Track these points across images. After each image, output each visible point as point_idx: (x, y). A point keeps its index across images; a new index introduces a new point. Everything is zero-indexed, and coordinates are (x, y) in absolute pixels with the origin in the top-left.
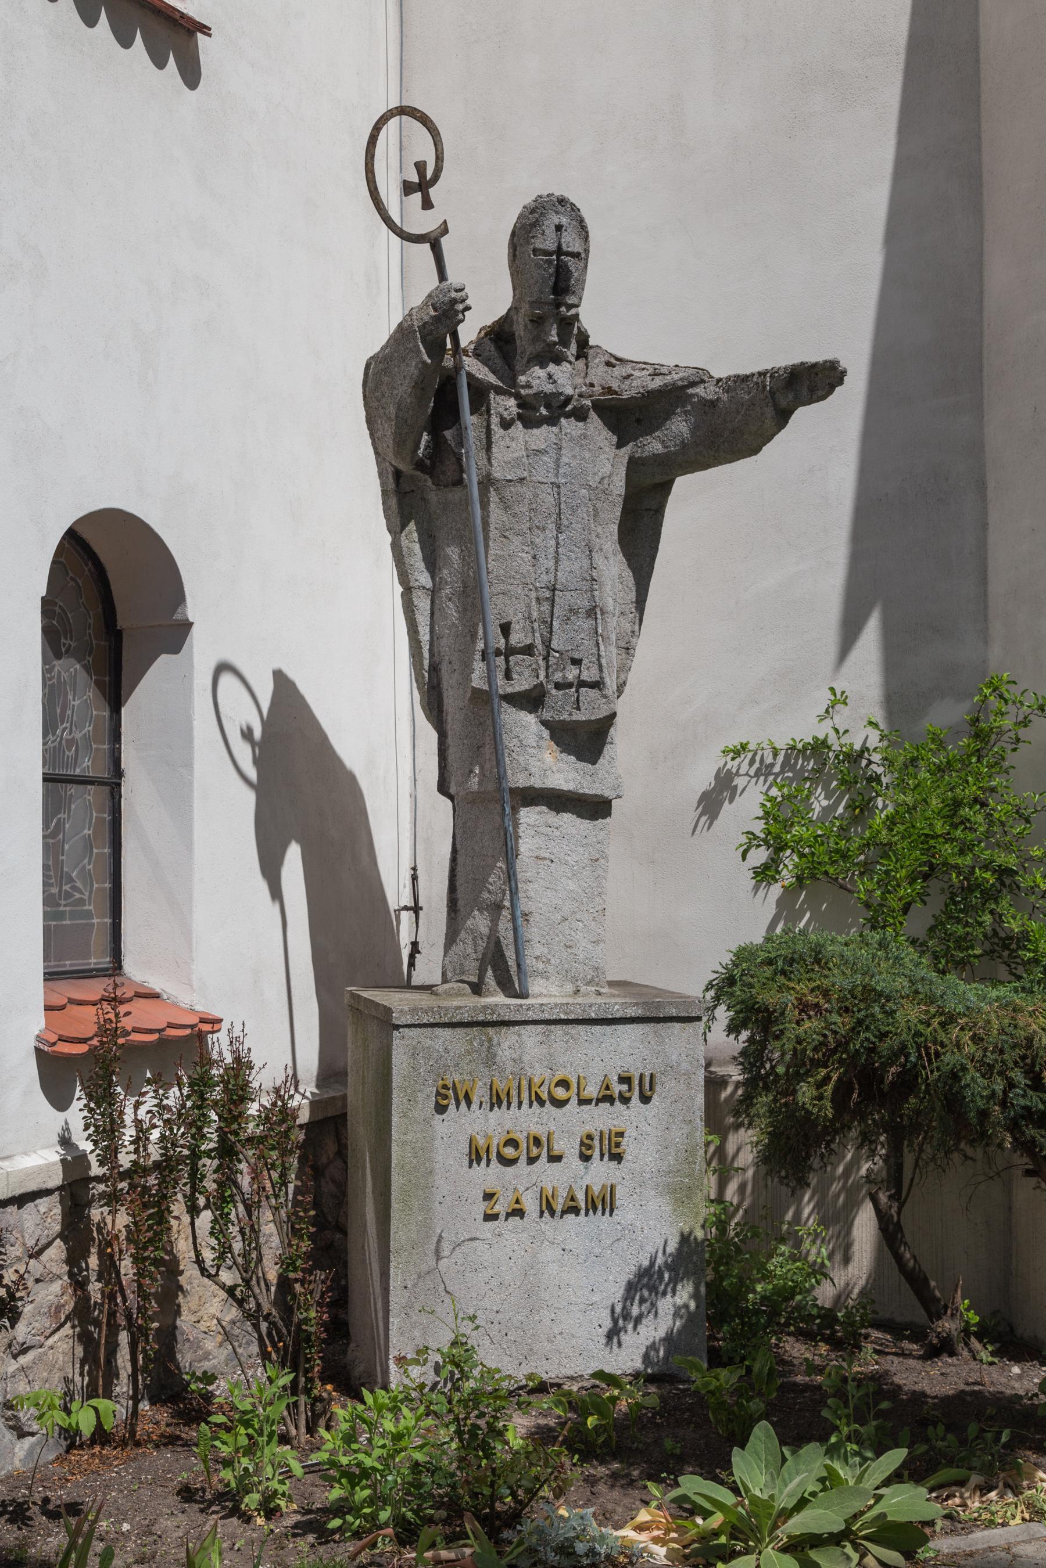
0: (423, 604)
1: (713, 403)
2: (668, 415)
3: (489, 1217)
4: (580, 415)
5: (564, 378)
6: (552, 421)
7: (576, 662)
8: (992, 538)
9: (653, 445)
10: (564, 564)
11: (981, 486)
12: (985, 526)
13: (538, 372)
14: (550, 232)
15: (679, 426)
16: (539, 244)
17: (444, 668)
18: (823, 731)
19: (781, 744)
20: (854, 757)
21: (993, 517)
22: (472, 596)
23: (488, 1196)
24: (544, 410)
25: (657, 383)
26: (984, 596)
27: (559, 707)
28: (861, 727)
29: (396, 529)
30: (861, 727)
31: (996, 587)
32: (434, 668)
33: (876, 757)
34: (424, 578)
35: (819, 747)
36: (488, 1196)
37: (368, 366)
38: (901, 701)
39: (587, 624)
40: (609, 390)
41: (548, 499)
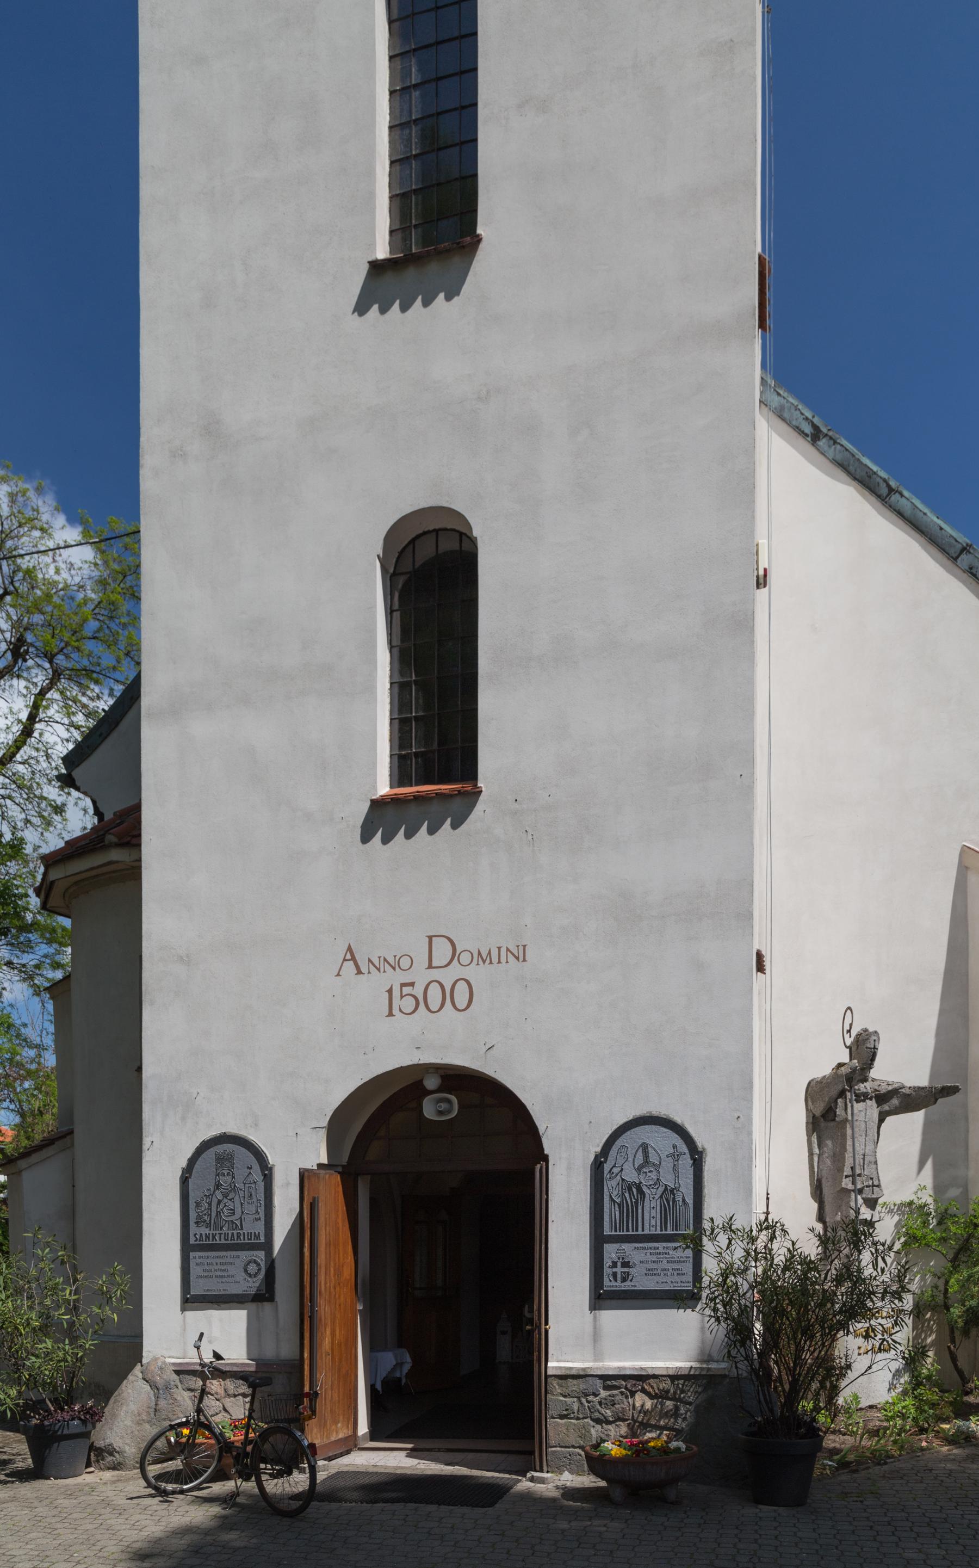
0: (816, 1159)
1: (909, 1095)
2: (892, 1098)
3: (859, 1354)
4: (871, 1099)
5: (862, 1087)
6: (864, 1101)
7: (872, 1179)
8: (971, 1135)
9: (886, 1107)
10: (868, 1148)
11: (967, 1119)
12: (968, 1131)
13: (862, 1085)
14: (872, 1042)
15: (895, 1102)
16: (868, 1045)
17: (824, 1181)
18: (913, 1197)
19: (898, 1202)
20: (922, 1207)
21: (971, 1128)
22: (838, 1158)
23: (859, 1348)
24: (862, 1097)
25: (890, 1088)
26: (967, 1154)
27: (867, 1193)
28: (927, 1198)
29: (809, 1136)
30: (927, 1198)
31: (971, 1152)
32: (819, 1181)
33: (931, 1206)
34: (816, 1151)
35: (911, 1203)
36: (859, 1348)
37: (809, 1083)
38: (939, 1189)
39: (874, 1166)
40: (876, 1090)
41: (863, 1126)
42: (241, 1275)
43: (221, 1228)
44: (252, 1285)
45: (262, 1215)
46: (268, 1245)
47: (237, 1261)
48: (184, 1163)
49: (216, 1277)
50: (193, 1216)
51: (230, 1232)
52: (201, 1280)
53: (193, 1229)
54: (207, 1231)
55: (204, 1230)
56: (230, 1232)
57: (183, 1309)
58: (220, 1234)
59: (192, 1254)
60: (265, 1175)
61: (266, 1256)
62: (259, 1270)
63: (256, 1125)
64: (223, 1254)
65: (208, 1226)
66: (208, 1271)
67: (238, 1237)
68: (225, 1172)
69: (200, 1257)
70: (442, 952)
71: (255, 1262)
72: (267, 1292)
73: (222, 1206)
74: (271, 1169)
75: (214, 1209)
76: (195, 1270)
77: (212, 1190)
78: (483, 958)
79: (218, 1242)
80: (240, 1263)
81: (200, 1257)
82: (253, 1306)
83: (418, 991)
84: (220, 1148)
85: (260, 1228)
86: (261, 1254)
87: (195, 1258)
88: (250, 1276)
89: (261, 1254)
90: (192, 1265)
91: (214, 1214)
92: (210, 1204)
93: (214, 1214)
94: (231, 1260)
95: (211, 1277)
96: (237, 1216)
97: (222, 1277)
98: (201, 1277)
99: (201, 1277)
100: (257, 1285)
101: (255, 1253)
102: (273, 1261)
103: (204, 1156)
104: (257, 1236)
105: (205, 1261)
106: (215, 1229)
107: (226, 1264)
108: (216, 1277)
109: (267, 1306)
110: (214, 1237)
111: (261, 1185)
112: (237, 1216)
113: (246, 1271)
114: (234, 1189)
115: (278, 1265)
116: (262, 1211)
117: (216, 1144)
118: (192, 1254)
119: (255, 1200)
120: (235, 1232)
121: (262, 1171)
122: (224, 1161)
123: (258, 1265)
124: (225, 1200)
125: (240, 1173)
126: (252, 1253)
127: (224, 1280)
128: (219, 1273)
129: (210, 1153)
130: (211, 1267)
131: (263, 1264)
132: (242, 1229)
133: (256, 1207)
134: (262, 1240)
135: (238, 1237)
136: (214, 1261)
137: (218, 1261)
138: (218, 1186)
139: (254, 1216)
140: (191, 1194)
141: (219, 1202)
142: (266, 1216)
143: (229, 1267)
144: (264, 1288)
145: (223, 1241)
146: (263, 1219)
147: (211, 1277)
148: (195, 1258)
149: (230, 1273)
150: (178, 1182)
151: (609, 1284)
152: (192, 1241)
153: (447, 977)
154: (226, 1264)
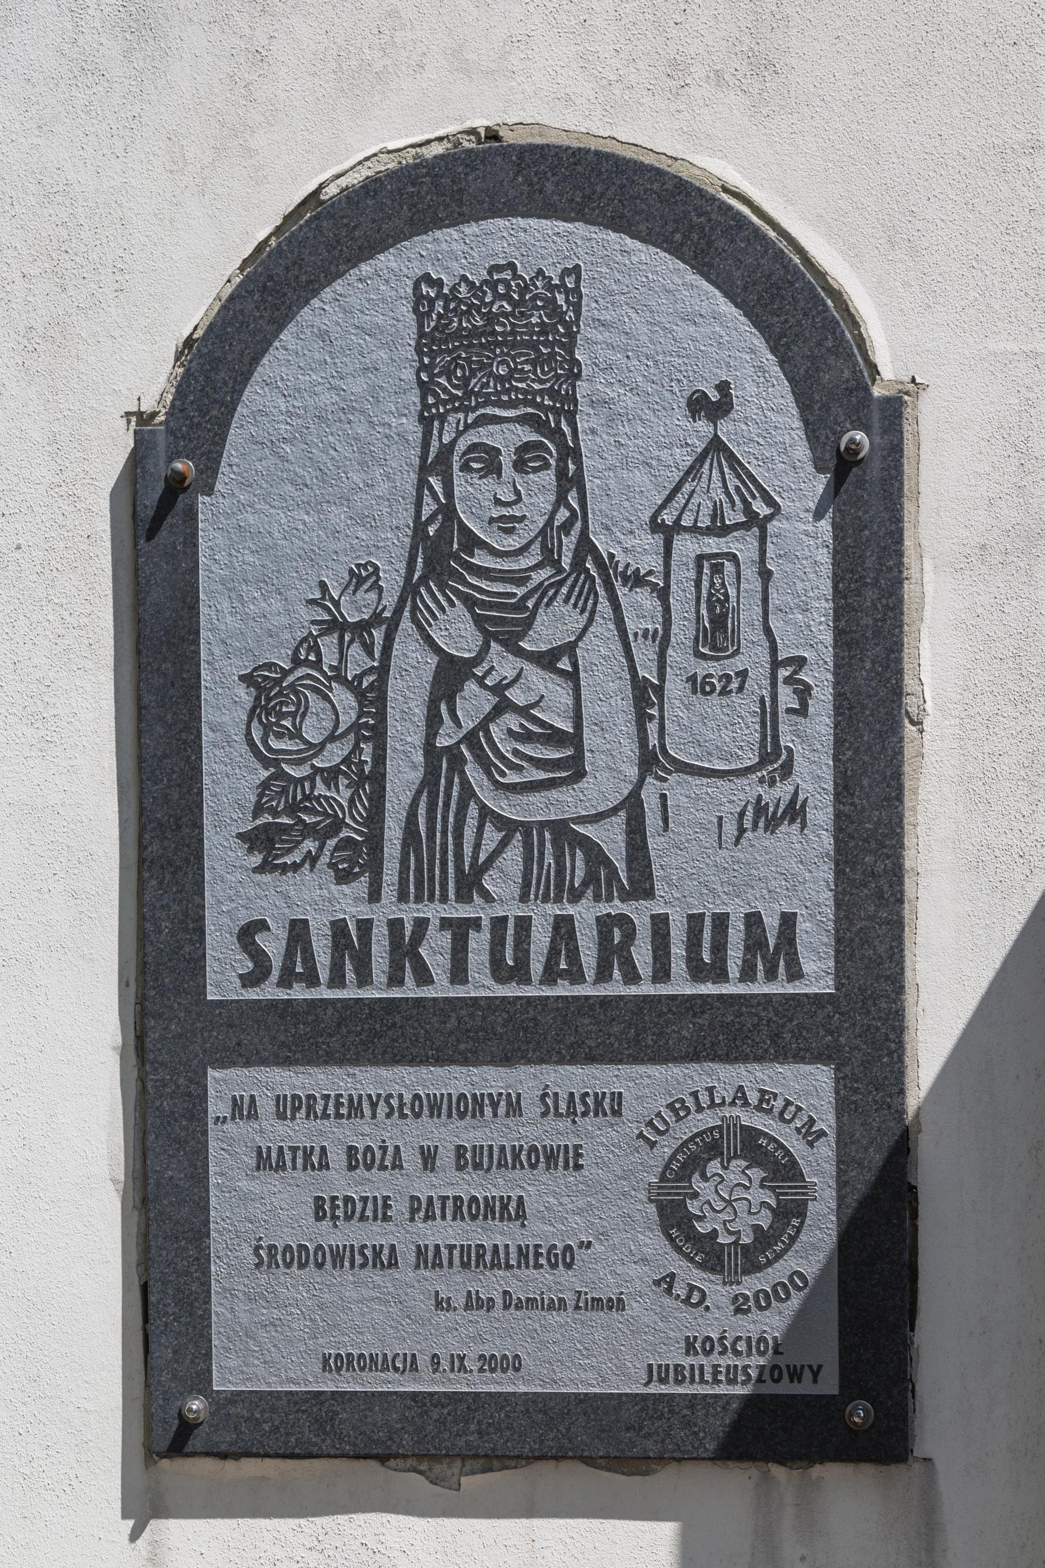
42: (632, 1252)
43: (470, 885)
44: (746, 1328)
45: (814, 775)
46: (863, 1021)
47: (597, 1136)
48: (149, 378)
49: (427, 1258)
50: (229, 783)
51: (542, 917)
52: (294, 1285)
53: (232, 886)
54: (349, 902)
55: (320, 898)
56: (542, 917)
57: (144, 1506)
58: (460, 930)
59: (223, 1084)
60: (842, 466)
61: (845, 1105)
62: (790, 1213)
63: (762, 65)
64: (491, 1079)
65: (360, 861)
66: (352, 1210)
67: (614, 953)
68: (507, 438)
69: (288, 1107)
71: (753, 1147)
72: (852, 1382)
73: (473, 702)
74: (891, 415)
75: (405, 734)
76: (247, 1205)
77: (392, 581)
79: (441, 989)
80: (620, 1164)
81: (288, 1107)
82: (732, 1489)
84: (461, 251)
85: (796, 878)
86: (810, 1087)
87: (243, 1109)
88: (710, 1255)
89: (810, 1087)
90: (227, 1151)
91: (403, 776)
92: (373, 696)
93: (403, 776)
94: (556, 1133)
95: (383, 1259)
96: (606, 781)
97: (474, 1258)
98: (298, 1257)
99: (298, 1257)
100: (773, 1323)
101: (753, 1076)
102: (902, 1148)
103: (320, 313)
104: (773, 947)
105: (337, 1136)
106: (418, 886)
107: (512, 1159)
108: (427, 1258)
109: (848, 1498)
110: (405, 950)
111: (805, 543)
112: (606, 781)
113: (675, 1219)
114: (590, 575)
115: (935, 1170)
116: (813, 747)
117: (424, 222)
118: (223, 1084)
119: (752, 657)
120: (585, 913)
121: (817, 425)
122: (499, 358)
123: (783, 1171)
124: (503, 665)
125: (632, 457)
126: (726, 1076)
127: (492, 1284)
128: (445, 1233)
129: (371, 307)
130: (376, 1184)
131: (819, 1165)
132: (642, 886)
133: (768, 717)
134: (817, 974)
135: (614, 953)
136: (410, 1135)
137: (446, 1135)
138: (440, 552)
139: (750, 789)
140: (216, 615)
141: (451, 675)
142: (844, 788)
143: (534, 1187)
144: (826, 1351)
145: (481, 984)
146: (821, 813)
147: (383, 1259)
148: (243, 1109)
149: (538, 1232)
150: (103, 526)
151: (266, 1341)
152: (224, 976)
154: (512, 1159)
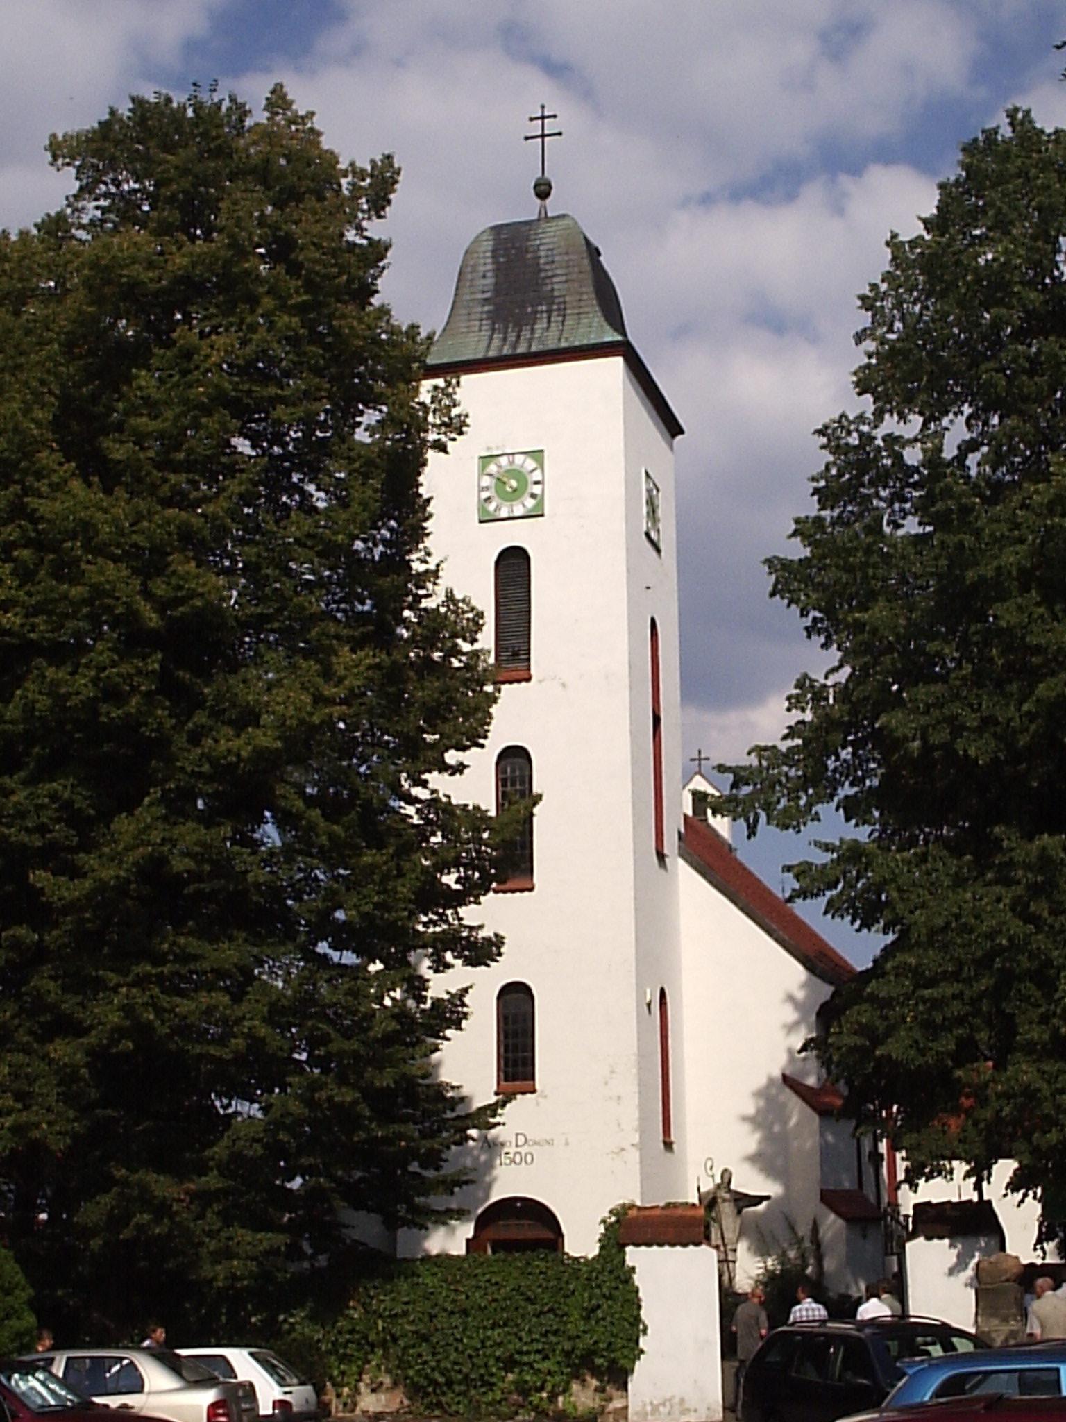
70: (521, 1140)
78: (536, 1143)
83: (511, 1156)
153: (523, 1150)
